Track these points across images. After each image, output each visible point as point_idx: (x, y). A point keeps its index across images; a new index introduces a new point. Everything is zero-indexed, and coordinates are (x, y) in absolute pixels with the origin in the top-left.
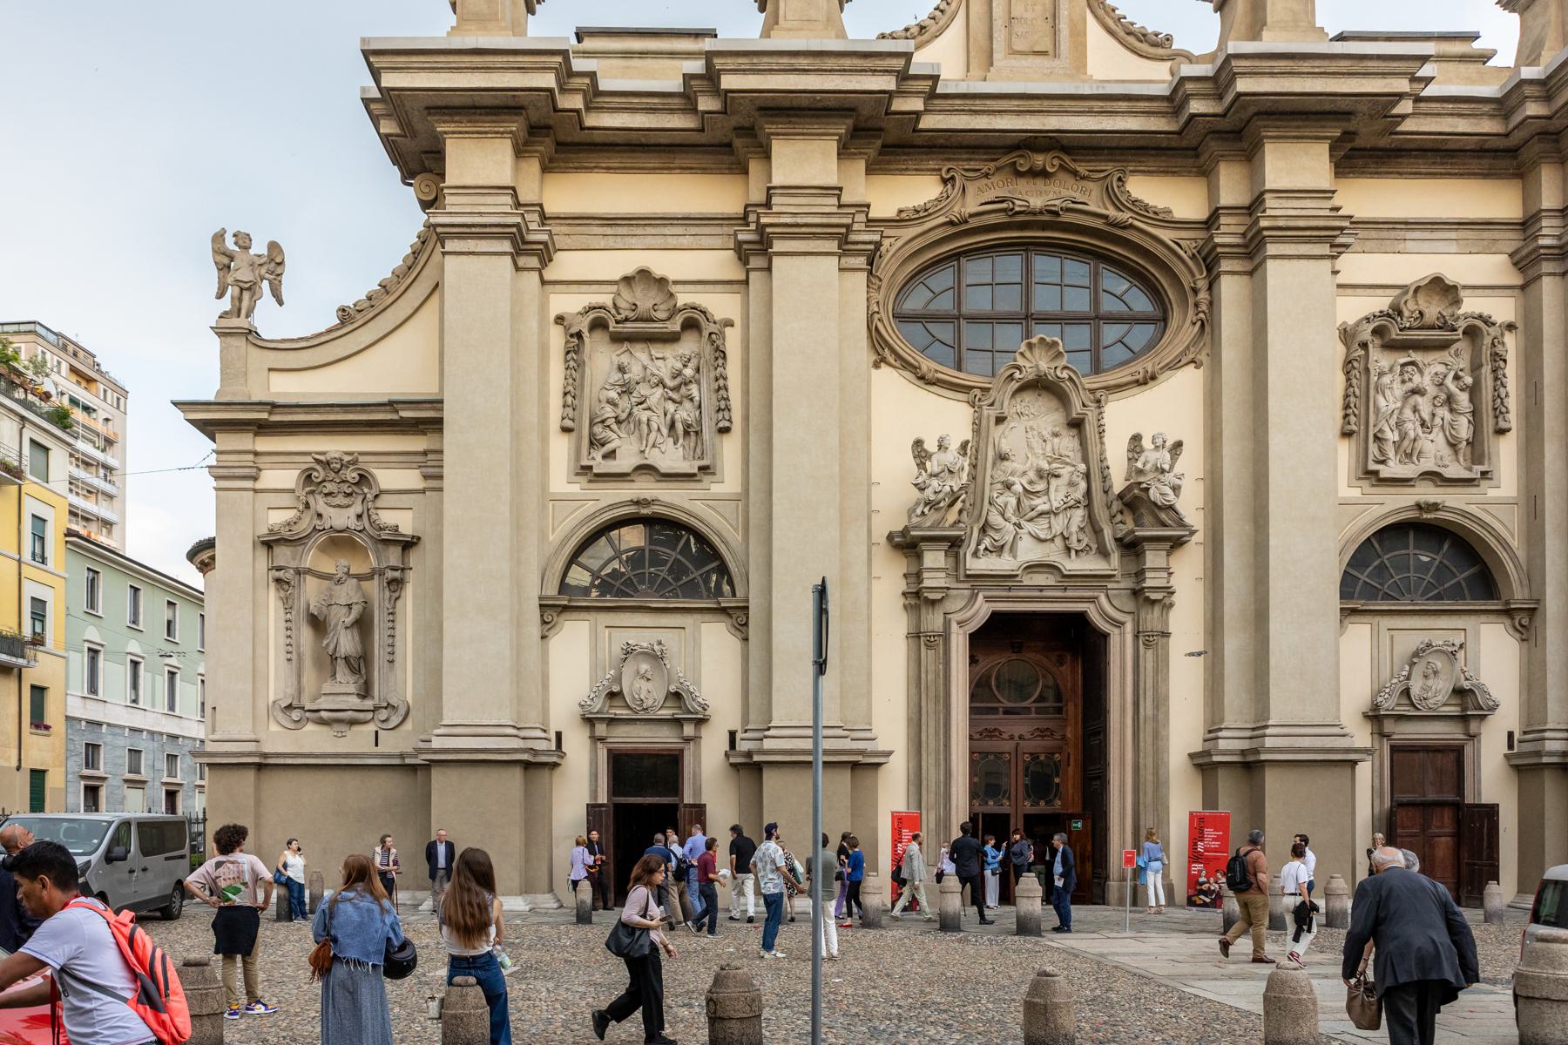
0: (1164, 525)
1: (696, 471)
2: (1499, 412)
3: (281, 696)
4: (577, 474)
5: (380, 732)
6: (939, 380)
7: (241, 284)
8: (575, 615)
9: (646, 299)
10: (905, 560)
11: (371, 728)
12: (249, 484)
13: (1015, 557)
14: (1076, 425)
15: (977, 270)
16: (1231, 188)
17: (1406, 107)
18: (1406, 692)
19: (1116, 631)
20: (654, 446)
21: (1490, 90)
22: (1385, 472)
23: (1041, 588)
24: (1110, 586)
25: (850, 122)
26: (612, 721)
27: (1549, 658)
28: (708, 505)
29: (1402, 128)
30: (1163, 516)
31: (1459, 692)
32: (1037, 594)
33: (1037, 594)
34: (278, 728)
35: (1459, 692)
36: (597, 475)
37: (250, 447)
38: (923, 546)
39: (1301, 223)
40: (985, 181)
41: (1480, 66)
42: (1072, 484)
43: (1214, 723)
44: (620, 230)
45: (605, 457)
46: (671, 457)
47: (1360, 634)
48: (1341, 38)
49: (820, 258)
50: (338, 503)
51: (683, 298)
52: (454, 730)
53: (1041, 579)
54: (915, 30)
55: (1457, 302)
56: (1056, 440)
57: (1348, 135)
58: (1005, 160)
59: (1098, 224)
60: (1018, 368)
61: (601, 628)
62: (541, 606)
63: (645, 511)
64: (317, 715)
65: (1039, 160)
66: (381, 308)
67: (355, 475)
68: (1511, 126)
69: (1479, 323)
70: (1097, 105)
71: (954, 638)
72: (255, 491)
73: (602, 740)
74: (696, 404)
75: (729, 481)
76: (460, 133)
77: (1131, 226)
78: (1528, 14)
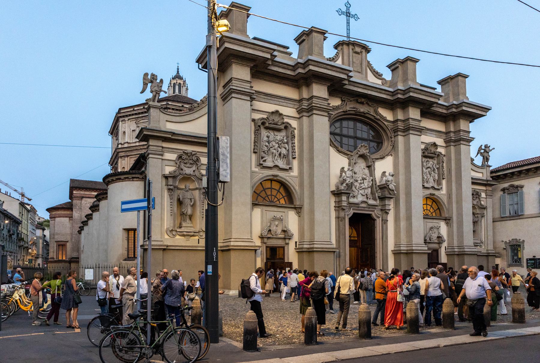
0: (390, 194)
1: (288, 168)
2: (443, 175)
3: (169, 227)
4: (258, 166)
5: (200, 239)
6: (342, 152)
7: (157, 92)
8: (257, 206)
9: (276, 119)
10: (334, 198)
11: (197, 238)
12: (160, 157)
13: (357, 199)
14: (369, 167)
15: (345, 123)
16: (400, 115)
17: (347, 82)
18: (270, 230)
19: (378, 219)
20: (276, 160)
21: (292, 63)
22: (265, 164)
23: (364, 208)
24: (377, 208)
25: (254, 63)
26: (269, 238)
27: (454, 230)
28: (290, 178)
29: (269, 68)
30: (391, 192)
31: (284, 231)
32: (363, 209)
33: (363, 209)
34: (168, 237)
35: (438, 237)
36: (264, 167)
37: (161, 145)
38: (168, 177)
39: (417, 127)
40: (350, 102)
41: (289, 56)
42: (369, 182)
43: (396, 243)
44: (268, 98)
45: (263, 161)
46: (281, 163)
47: (257, 211)
48: (255, 38)
49: (324, 117)
50: (188, 166)
51: (286, 120)
52: (237, 240)
53: (363, 205)
54: (332, 59)
55: (437, 149)
56: (364, 170)
57: (255, 66)
58: (355, 98)
59: (373, 118)
60: (359, 151)
61: (264, 211)
62: (252, 203)
63: (275, 178)
64: (182, 233)
65: (363, 100)
66: (202, 107)
67: (195, 158)
68: (448, 112)
69: (440, 154)
70: (379, 90)
71: (346, 219)
72: (162, 159)
73: (265, 243)
74: (287, 150)
75: (295, 172)
76: (237, 63)
77: (380, 120)
78: (444, 86)
